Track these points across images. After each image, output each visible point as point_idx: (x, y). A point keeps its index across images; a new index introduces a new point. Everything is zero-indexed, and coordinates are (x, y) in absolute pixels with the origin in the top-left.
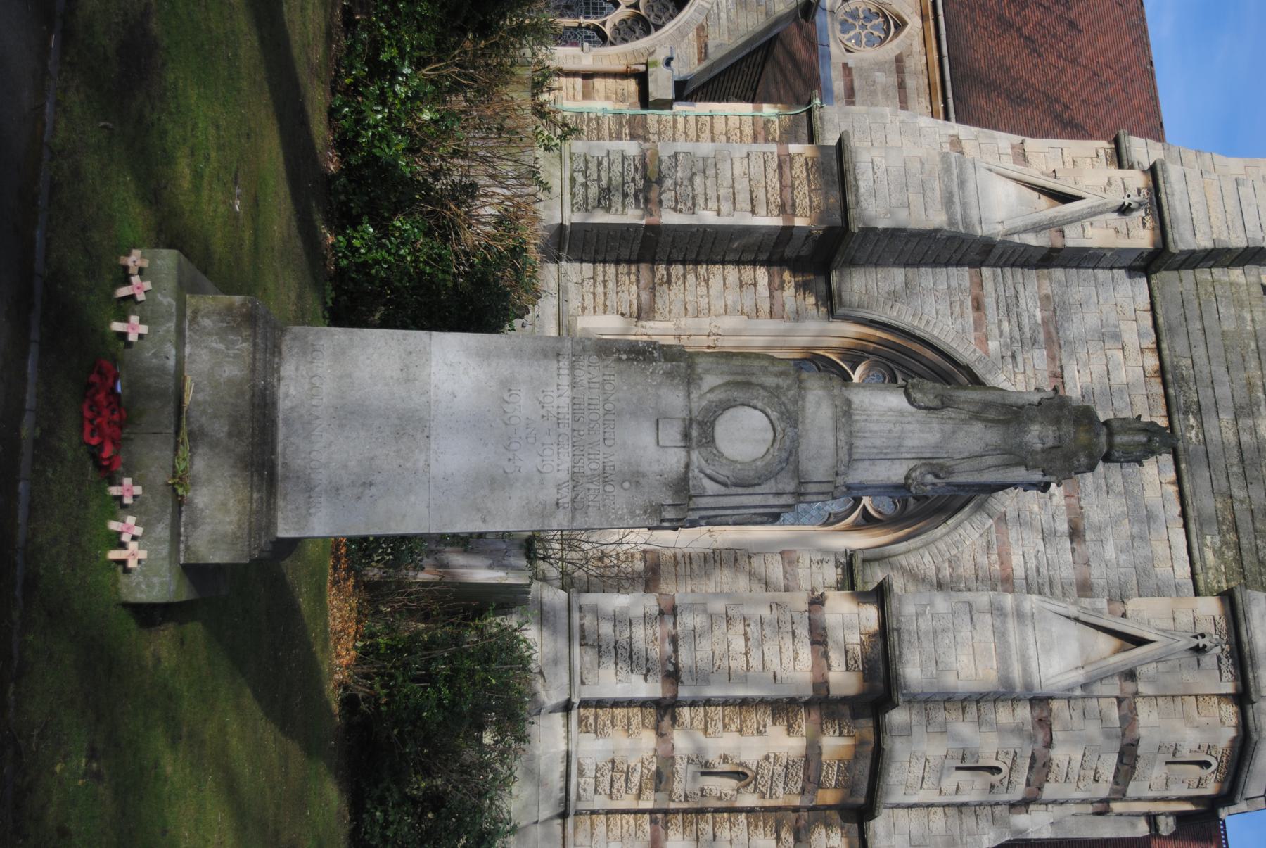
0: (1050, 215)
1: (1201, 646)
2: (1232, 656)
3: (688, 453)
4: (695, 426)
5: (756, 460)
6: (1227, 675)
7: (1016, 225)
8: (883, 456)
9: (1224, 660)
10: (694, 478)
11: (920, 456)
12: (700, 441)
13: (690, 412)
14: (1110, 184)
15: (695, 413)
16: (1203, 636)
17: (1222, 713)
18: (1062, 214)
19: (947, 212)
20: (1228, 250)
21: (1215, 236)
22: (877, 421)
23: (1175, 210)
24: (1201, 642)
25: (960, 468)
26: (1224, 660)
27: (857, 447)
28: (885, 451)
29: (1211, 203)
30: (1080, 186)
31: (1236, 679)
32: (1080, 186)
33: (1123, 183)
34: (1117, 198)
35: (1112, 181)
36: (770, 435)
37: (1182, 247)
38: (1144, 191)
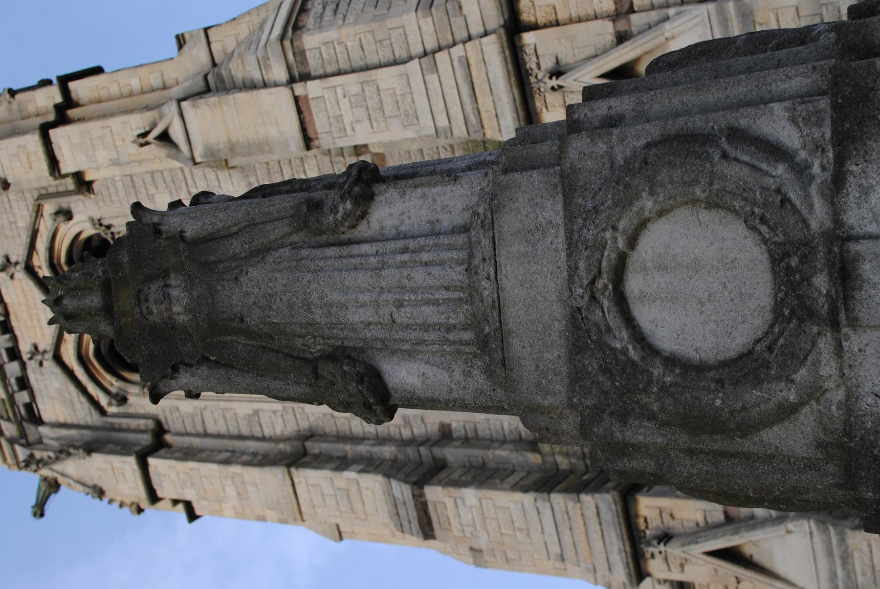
0: (737, 537)
1: (554, 78)
2: (527, 71)
3: (837, 222)
4: (822, 305)
5: (661, 214)
6: (529, 50)
7: (774, 529)
8: (412, 244)
9: (534, 66)
10: (818, 148)
11: (345, 251)
12: (804, 259)
13: (839, 347)
14: (682, 566)
15: (825, 344)
16: (553, 88)
17: (533, 11)
18: (727, 538)
19: (847, 547)
20: (566, 491)
21: (579, 505)
22: (427, 327)
23: (617, 535)
24: (554, 82)
25: (283, 228)
26: (534, 66)
27: (459, 263)
28: (406, 257)
29: (584, 538)
30: (711, 567)
31: (522, 47)
32: (711, 567)
33: (668, 565)
34: (674, 550)
35: (679, 569)
36: (634, 284)
37: (608, 497)
38: (648, 555)
